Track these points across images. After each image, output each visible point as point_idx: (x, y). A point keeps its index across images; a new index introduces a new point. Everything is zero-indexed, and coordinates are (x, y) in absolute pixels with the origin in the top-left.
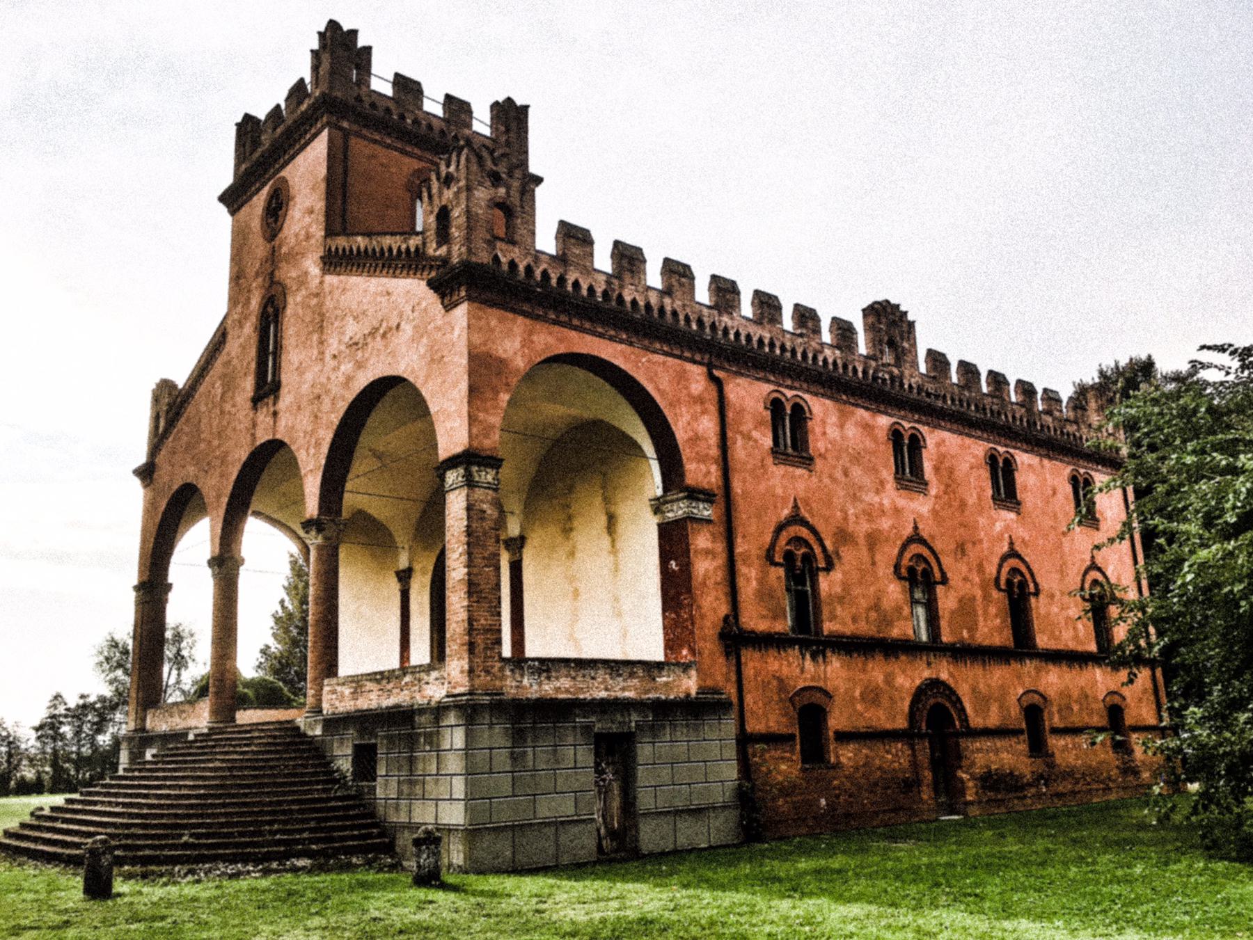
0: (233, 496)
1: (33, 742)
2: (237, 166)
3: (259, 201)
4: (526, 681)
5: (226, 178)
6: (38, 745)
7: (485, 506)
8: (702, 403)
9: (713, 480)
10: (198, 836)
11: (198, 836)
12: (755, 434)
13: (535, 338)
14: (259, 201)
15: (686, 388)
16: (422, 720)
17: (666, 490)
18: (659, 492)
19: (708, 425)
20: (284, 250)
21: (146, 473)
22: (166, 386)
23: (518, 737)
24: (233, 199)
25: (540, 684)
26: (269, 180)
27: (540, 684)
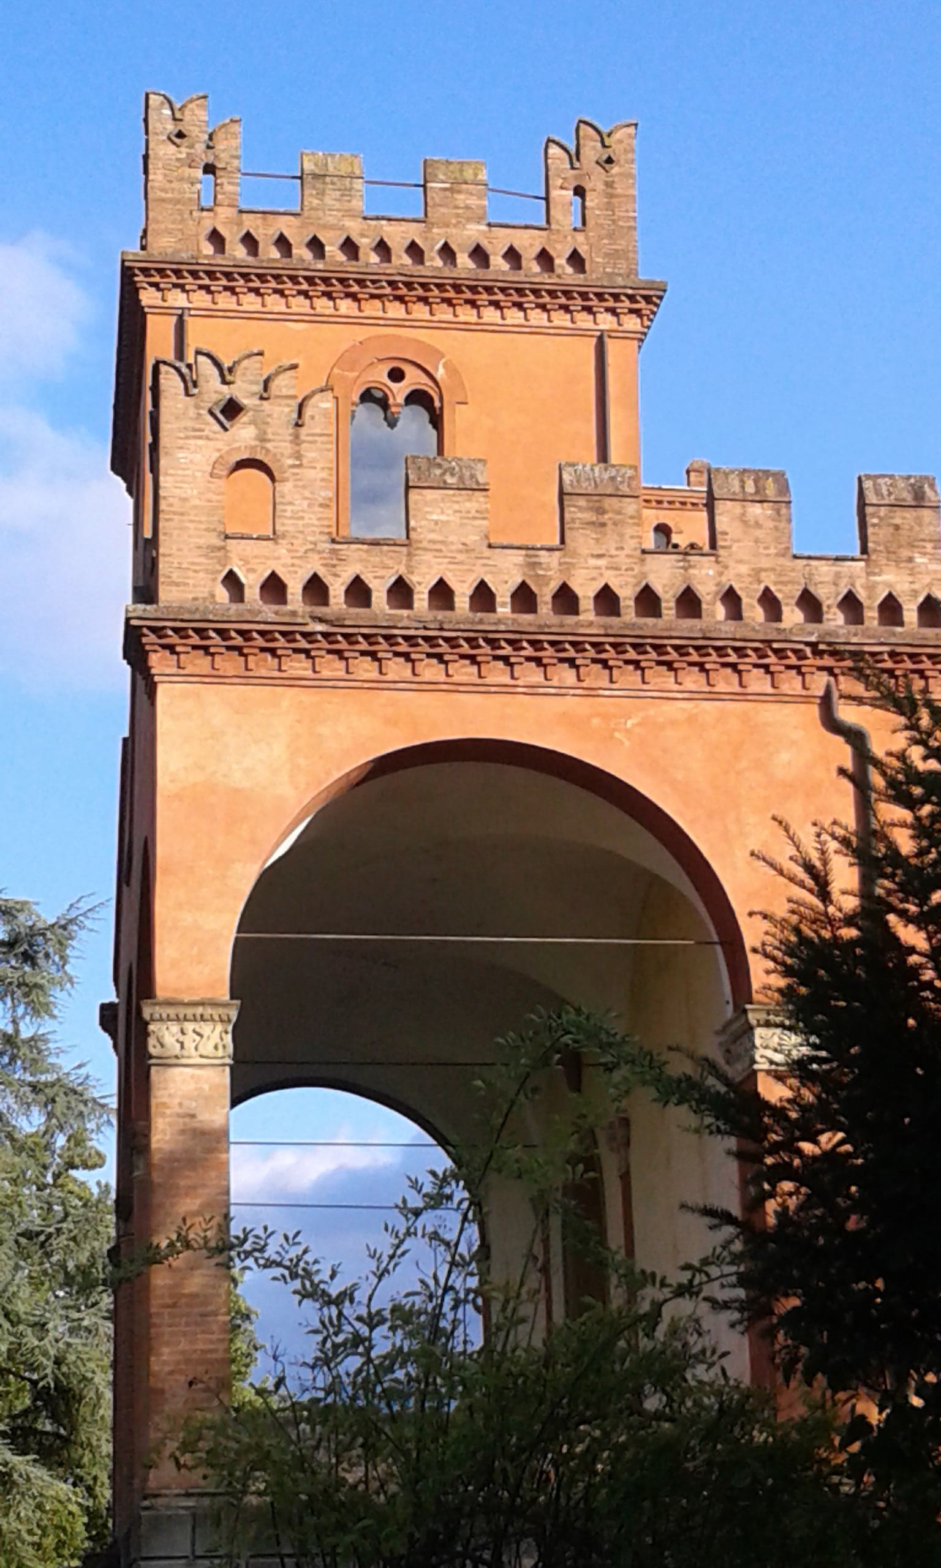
13: (324, 730)
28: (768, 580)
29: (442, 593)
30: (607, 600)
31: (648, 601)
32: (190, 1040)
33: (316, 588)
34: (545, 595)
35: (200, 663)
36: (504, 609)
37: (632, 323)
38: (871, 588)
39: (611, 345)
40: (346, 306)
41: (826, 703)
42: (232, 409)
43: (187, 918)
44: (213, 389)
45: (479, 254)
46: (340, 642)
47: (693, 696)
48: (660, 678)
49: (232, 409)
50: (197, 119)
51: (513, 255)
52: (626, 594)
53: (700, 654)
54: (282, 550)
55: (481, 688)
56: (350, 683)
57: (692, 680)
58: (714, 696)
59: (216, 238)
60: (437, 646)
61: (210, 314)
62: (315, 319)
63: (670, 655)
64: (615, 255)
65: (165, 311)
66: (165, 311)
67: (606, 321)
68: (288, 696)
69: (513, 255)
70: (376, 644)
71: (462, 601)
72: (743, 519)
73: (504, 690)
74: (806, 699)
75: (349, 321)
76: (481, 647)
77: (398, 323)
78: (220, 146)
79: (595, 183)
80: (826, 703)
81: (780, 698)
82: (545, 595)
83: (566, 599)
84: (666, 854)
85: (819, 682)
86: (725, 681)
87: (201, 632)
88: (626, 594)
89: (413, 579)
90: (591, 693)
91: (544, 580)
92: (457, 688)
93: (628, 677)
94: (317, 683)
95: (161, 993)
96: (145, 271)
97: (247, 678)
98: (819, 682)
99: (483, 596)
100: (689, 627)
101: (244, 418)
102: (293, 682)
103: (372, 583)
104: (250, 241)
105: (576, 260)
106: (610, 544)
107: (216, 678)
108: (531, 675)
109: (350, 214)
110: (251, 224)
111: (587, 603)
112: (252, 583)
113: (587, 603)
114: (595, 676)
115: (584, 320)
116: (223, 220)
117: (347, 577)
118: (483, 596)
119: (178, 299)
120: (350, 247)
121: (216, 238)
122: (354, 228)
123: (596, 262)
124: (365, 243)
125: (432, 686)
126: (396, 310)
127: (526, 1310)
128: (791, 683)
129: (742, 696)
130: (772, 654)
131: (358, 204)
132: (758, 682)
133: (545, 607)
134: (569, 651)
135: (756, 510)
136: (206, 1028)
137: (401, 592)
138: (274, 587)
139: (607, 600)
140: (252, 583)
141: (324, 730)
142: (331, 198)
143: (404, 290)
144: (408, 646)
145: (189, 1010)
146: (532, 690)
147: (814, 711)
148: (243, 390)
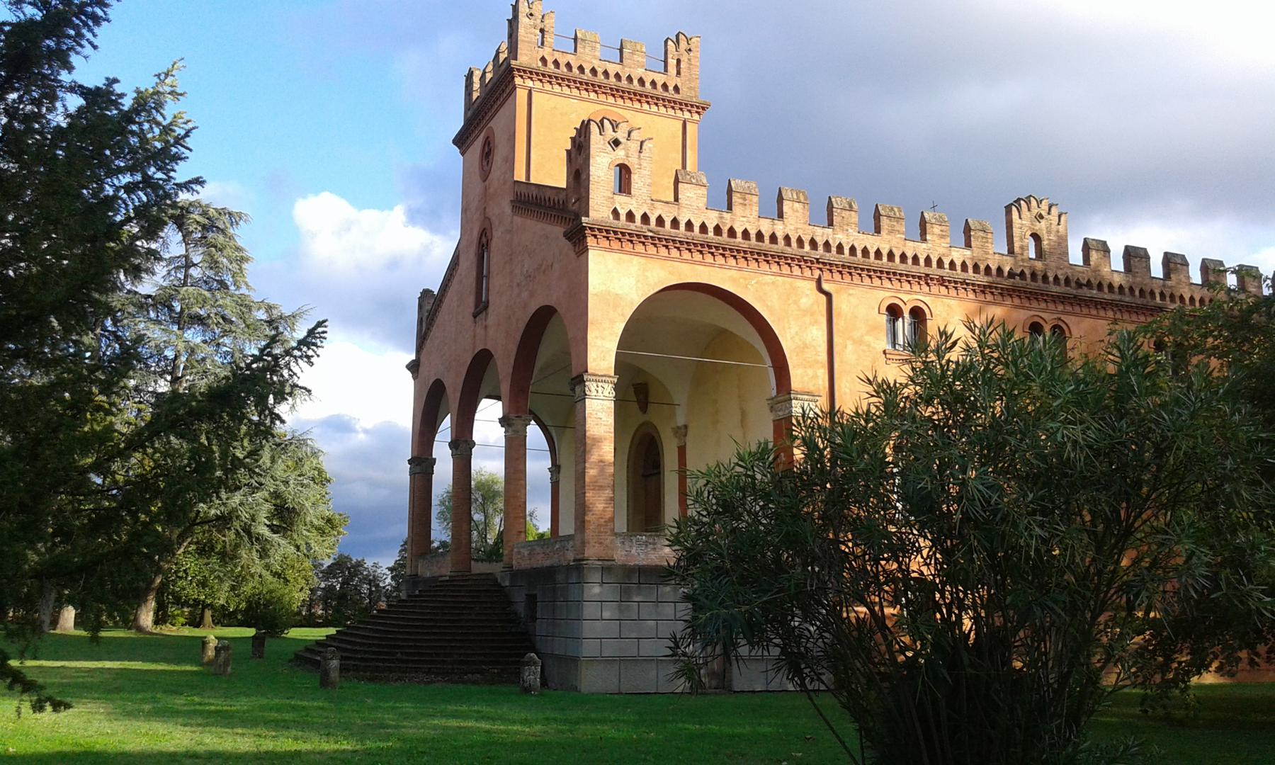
0: (516, 367)
1: (388, 581)
2: (466, 113)
3: (477, 145)
4: (633, 551)
5: (458, 123)
6: (393, 583)
7: (600, 415)
8: (812, 314)
9: (820, 382)
10: (407, 654)
11: (407, 654)
12: (868, 338)
13: (648, 274)
14: (477, 145)
15: (795, 302)
16: (560, 578)
17: (778, 392)
18: (774, 393)
19: (818, 334)
20: (491, 190)
21: (414, 367)
22: (426, 293)
23: (624, 598)
24: (462, 141)
25: (647, 554)
26: (481, 131)
27: (647, 554)
28: (800, 233)
29: (689, 225)
30: (746, 234)
31: (760, 236)
32: (600, 389)
33: (645, 218)
34: (725, 230)
35: (605, 243)
36: (711, 234)
37: (696, 117)
38: (834, 239)
39: (689, 126)
40: (593, 95)
41: (819, 281)
42: (616, 143)
43: (599, 342)
44: (1035, 211)
45: (641, 82)
46: (656, 241)
47: (775, 274)
48: (764, 266)
49: (616, 143)
50: (538, 9)
51: (653, 83)
52: (753, 233)
53: (780, 259)
54: (634, 201)
55: (703, 263)
56: (657, 256)
57: (775, 268)
58: (782, 275)
59: (543, 60)
60: (690, 246)
61: (541, 91)
62: (582, 99)
63: (767, 257)
64: (690, 88)
65: (524, 87)
66: (524, 87)
67: (687, 115)
68: (636, 260)
69: (653, 83)
70: (668, 242)
71: (697, 229)
72: (792, 208)
73: (712, 265)
74: (811, 279)
75: (593, 101)
76: (705, 248)
77: (612, 105)
78: (547, 21)
79: (684, 59)
80: (819, 281)
81: (804, 278)
82: (725, 230)
83: (732, 232)
84: (757, 335)
85: (817, 273)
86: (786, 269)
87: (607, 231)
88: (753, 233)
89: (679, 218)
90: (740, 269)
91: (725, 224)
92: (695, 263)
93: (753, 264)
94: (646, 256)
95: (590, 371)
96: (519, 70)
97: (622, 251)
98: (817, 273)
99: (703, 228)
100: (903, 267)
101: (621, 147)
102: (637, 254)
103: (665, 219)
104: (556, 63)
105: (676, 89)
106: (747, 213)
107: (611, 250)
108: (720, 260)
109: (595, 57)
110: (557, 56)
111: (739, 235)
112: (623, 213)
113: (739, 235)
114: (742, 263)
115: (679, 113)
116: (546, 52)
117: (656, 215)
118: (703, 228)
119: (529, 83)
120: (594, 71)
121: (543, 60)
122: (596, 64)
123: (683, 90)
124: (600, 71)
125: (686, 261)
126: (611, 100)
127: (1148, 530)
128: (807, 273)
129: (791, 276)
130: (802, 261)
131: (598, 54)
132: (797, 271)
133: (725, 234)
134: (735, 253)
135: (797, 205)
136: (606, 386)
137: (675, 223)
138: (630, 216)
139: (746, 234)
140: (623, 213)
141: (648, 274)
142: (588, 50)
143: (616, 92)
144: (679, 244)
145: (599, 378)
146: (721, 266)
147: (814, 284)
148: (621, 135)
